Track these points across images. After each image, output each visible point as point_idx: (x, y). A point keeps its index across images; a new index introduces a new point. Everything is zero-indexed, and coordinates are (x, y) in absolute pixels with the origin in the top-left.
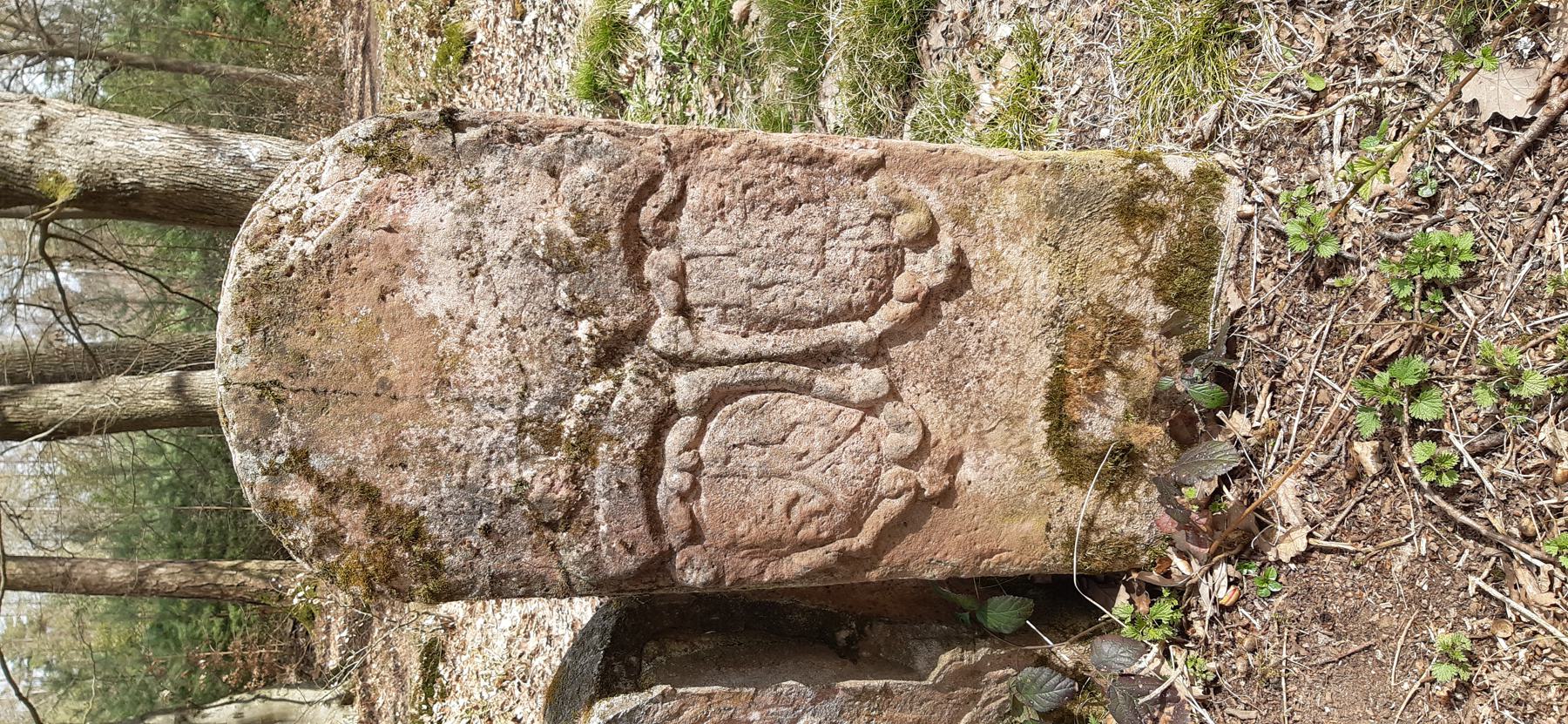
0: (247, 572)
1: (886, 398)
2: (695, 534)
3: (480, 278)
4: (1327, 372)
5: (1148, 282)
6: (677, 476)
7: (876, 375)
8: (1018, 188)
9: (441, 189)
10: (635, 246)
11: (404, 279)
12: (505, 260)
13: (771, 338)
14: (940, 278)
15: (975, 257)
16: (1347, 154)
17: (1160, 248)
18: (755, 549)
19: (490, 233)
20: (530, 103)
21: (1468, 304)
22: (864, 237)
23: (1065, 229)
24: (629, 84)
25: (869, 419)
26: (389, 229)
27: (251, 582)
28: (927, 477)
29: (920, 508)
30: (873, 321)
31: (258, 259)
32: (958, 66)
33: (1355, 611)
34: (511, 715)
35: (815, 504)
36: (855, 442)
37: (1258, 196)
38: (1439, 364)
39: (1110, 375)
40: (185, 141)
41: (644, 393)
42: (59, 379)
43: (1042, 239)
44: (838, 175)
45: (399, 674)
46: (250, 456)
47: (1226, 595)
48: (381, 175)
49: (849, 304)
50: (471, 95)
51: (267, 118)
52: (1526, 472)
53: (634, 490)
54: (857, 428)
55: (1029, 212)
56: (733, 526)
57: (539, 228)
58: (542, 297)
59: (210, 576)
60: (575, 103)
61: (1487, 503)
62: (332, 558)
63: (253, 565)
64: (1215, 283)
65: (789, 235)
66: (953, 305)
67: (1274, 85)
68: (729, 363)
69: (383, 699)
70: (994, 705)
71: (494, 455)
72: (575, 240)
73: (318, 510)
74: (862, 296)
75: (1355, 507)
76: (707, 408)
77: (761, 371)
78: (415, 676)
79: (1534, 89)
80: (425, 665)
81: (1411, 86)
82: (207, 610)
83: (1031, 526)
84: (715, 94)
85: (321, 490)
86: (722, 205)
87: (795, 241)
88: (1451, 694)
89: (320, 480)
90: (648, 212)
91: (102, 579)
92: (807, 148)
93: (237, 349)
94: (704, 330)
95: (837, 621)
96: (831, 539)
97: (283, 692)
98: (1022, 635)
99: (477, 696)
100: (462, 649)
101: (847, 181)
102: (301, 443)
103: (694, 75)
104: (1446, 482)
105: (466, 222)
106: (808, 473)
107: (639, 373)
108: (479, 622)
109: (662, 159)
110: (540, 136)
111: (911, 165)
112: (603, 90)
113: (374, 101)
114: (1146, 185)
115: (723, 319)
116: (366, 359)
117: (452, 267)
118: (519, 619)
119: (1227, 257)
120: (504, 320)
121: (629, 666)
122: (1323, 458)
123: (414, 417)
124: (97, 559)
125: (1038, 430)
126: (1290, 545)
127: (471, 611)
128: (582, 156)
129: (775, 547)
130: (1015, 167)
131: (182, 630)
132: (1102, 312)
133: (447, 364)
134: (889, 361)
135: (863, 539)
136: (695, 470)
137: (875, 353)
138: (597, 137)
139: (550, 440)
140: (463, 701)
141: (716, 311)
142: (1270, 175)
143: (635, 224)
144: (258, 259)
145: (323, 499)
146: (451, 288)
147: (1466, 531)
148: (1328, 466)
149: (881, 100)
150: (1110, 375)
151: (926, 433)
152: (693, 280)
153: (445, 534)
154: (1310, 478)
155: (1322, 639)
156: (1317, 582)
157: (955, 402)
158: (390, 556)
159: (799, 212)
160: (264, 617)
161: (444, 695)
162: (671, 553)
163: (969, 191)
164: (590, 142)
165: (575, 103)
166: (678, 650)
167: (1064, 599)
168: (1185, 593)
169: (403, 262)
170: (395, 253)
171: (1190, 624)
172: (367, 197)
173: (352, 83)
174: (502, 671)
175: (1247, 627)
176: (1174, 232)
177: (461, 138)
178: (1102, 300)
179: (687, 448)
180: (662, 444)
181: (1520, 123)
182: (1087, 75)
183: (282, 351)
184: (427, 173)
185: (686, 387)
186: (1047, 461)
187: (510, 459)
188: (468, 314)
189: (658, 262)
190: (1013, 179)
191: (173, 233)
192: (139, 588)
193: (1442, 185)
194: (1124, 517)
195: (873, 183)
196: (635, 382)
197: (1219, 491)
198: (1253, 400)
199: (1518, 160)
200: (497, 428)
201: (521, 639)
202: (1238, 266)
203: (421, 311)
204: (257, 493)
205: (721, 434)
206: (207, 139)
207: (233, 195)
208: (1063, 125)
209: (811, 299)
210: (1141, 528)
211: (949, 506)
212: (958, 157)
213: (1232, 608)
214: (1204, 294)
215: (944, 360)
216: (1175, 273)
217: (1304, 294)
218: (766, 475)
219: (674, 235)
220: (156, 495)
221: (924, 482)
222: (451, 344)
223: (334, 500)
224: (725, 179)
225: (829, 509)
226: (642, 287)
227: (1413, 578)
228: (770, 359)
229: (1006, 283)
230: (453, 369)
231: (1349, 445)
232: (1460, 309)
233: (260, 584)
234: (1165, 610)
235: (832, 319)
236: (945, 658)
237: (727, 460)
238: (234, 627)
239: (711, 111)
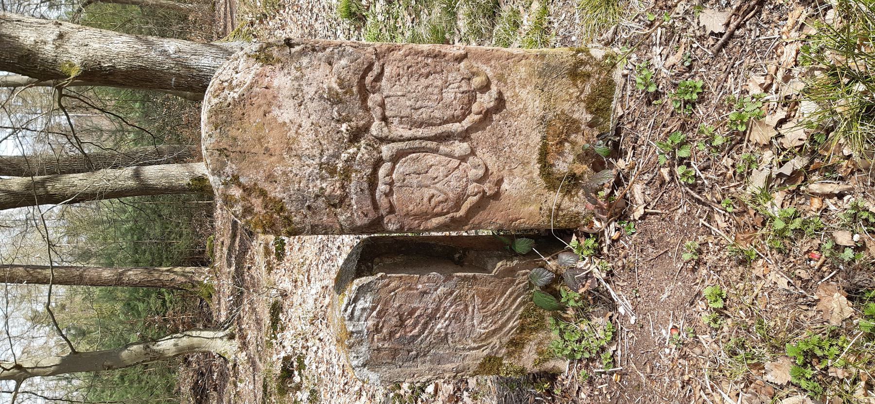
0: (175, 273)
1: (469, 155)
2: (392, 210)
3: (303, 107)
4: (653, 140)
5: (583, 105)
6: (384, 186)
7: (465, 145)
8: (525, 65)
9: (286, 71)
10: (364, 93)
11: (273, 108)
12: (312, 99)
13: (421, 130)
14: (492, 104)
15: (507, 95)
16: (662, 48)
17: (588, 89)
18: (416, 216)
19: (306, 88)
20: (316, 20)
21: (701, 109)
22: (459, 87)
23: (546, 82)
24: (368, 9)
25: (463, 163)
26: (266, 88)
27: (178, 278)
28: (488, 187)
29: (485, 201)
30: (464, 123)
31: (216, 100)
32: (515, 7)
33: (662, 238)
34: (318, 337)
35: (440, 198)
36: (457, 173)
37: (630, 67)
38: (690, 134)
39: (566, 144)
40: (136, 43)
41: (369, 153)
42: (74, 171)
43: (536, 87)
44: (447, 61)
45: (258, 322)
46: (216, 178)
47: (615, 235)
48: (262, 66)
49: (453, 116)
50: (285, 15)
51: (174, 28)
52: (718, 176)
53: (366, 192)
54: (458, 167)
55: (530, 75)
56: (407, 207)
57: (325, 86)
58: (327, 114)
59: (156, 275)
60: (340, 19)
61: (706, 189)
62: (249, 218)
63: (178, 269)
64: (613, 106)
65: (427, 87)
66: (498, 116)
67: (636, 18)
68: (404, 141)
69: (251, 335)
70: (521, 285)
71: (310, 178)
72: (340, 91)
73: (243, 199)
74: (458, 112)
75: (662, 195)
76: (395, 159)
77: (417, 144)
78: (267, 320)
79: (725, 21)
80: (273, 315)
81: (684, 19)
82: (153, 295)
83: (534, 208)
84: (410, 15)
85: (244, 191)
86: (399, 75)
87: (430, 89)
88: (693, 267)
89: (244, 187)
90: (369, 79)
91: (100, 277)
92: (434, 50)
93: (210, 136)
94: (393, 127)
95: (454, 250)
96: (448, 213)
97: (198, 332)
98: (530, 254)
99: (300, 329)
100: (291, 306)
101: (451, 64)
102: (236, 173)
103: (400, 5)
104: (690, 182)
105: (296, 84)
106: (438, 185)
107: (367, 145)
108: (300, 291)
109: (374, 57)
110: (324, 49)
111: (479, 56)
112: (354, 13)
113: (232, 19)
114: (582, 63)
115: (401, 123)
116: (259, 140)
117: (291, 103)
118: (320, 289)
119: (618, 93)
120: (312, 124)
121: (368, 267)
122: (651, 176)
123: (279, 162)
124: (94, 269)
125: (536, 168)
126: (639, 212)
127: (295, 286)
128: (341, 56)
129: (425, 216)
130: (524, 56)
131: (141, 306)
132: (563, 117)
133: (291, 141)
134: (471, 139)
135: (462, 212)
136: (391, 184)
137: (465, 136)
138: (347, 48)
139: (333, 172)
140: (292, 332)
141: (398, 119)
142: (634, 57)
143: (363, 84)
144: (216, 100)
145: (245, 195)
146: (291, 111)
147: (699, 201)
148: (652, 179)
149: (482, 23)
150: (566, 144)
151: (487, 169)
152: (388, 106)
153: (293, 209)
154: (647, 184)
155: (650, 250)
156: (649, 227)
157: (499, 156)
158: (271, 217)
159: (431, 77)
160: (183, 298)
161: (282, 329)
162: (382, 217)
163: (504, 67)
164: (344, 50)
165: (340, 19)
166: (388, 261)
167: (550, 239)
168: (599, 236)
169: (272, 101)
170: (269, 97)
171: (602, 248)
172: (257, 75)
173: (220, 8)
174: (312, 315)
175: (623, 248)
176: (594, 82)
177: (293, 50)
178: (563, 113)
179: (387, 175)
180: (377, 174)
181: (721, 34)
182: (568, 12)
183: (227, 137)
184: (280, 65)
185: (386, 150)
186: (540, 181)
187: (317, 179)
188: (299, 121)
189: (373, 99)
190: (523, 61)
191: (124, 93)
192: (118, 282)
193: (694, 60)
194: (574, 204)
195: (462, 64)
196: (365, 148)
197: (612, 192)
198: (626, 153)
199: (719, 50)
200: (311, 167)
201: (321, 298)
202: (623, 96)
203: (280, 120)
204: (220, 192)
205: (401, 170)
206: (147, 42)
207: (161, 71)
208: (557, 35)
209: (437, 114)
210: (581, 209)
211: (498, 200)
212: (499, 53)
213: (617, 240)
214: (608, 109)
215: (494, 139)
216: (595, 100)
217: (645, 108)
218: (420, 186)
219: (379, 89)
220: (124, 235)
221: (487, 190)
222: (292, 133)
223: (249, 195)
224: (400, 64)
225: (446, 200)
226: (367, 110)
227: (682, 222)
228: (421, 139)
229: (521, 106)
230: (293, 143)
231: (659, 170)
232: (698, 112)
233: (183, 279)
234: (591, 242)
235: (446, 122)
236: (499, 264)
237: (404, 180)
238: (168, 304)
239: (409, 24)
